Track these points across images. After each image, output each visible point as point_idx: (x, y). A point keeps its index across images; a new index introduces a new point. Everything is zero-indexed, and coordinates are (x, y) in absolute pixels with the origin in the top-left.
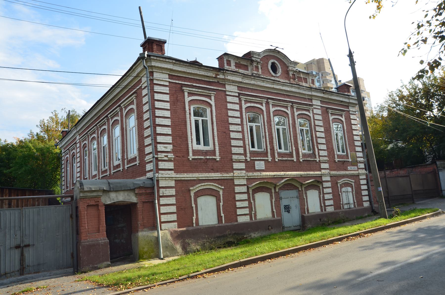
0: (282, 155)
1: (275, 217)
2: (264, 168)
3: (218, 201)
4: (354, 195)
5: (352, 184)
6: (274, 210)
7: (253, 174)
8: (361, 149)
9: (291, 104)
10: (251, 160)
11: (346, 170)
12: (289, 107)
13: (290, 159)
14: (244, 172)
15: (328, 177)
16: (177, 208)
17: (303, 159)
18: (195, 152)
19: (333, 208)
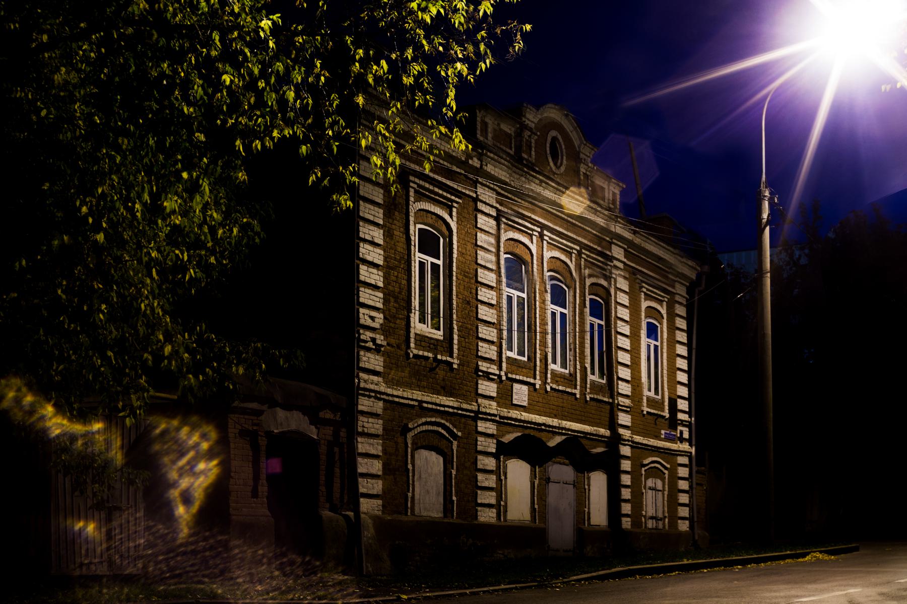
0: (558, 379)
1: (536, 523)
2: (527, 402)
3: (447, 463)
4: (666, 499)
5: (664, 474)
6: (536, 506)
7: (509, 412)
8: (687, 392)
9: (578, 248)
10: (508, 378)
11: (657, 437)
12: (573, 255)
13: (569, 390)
14: (494, 404)
15: (628, 447)
16: (385, 467)
17: (590, 396)
18: (422, 340)
19: (630, 523)
